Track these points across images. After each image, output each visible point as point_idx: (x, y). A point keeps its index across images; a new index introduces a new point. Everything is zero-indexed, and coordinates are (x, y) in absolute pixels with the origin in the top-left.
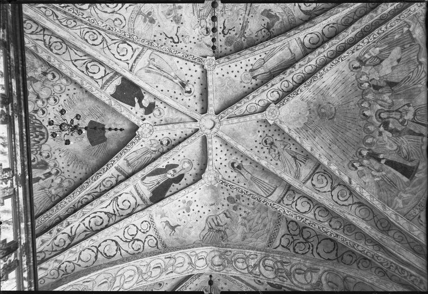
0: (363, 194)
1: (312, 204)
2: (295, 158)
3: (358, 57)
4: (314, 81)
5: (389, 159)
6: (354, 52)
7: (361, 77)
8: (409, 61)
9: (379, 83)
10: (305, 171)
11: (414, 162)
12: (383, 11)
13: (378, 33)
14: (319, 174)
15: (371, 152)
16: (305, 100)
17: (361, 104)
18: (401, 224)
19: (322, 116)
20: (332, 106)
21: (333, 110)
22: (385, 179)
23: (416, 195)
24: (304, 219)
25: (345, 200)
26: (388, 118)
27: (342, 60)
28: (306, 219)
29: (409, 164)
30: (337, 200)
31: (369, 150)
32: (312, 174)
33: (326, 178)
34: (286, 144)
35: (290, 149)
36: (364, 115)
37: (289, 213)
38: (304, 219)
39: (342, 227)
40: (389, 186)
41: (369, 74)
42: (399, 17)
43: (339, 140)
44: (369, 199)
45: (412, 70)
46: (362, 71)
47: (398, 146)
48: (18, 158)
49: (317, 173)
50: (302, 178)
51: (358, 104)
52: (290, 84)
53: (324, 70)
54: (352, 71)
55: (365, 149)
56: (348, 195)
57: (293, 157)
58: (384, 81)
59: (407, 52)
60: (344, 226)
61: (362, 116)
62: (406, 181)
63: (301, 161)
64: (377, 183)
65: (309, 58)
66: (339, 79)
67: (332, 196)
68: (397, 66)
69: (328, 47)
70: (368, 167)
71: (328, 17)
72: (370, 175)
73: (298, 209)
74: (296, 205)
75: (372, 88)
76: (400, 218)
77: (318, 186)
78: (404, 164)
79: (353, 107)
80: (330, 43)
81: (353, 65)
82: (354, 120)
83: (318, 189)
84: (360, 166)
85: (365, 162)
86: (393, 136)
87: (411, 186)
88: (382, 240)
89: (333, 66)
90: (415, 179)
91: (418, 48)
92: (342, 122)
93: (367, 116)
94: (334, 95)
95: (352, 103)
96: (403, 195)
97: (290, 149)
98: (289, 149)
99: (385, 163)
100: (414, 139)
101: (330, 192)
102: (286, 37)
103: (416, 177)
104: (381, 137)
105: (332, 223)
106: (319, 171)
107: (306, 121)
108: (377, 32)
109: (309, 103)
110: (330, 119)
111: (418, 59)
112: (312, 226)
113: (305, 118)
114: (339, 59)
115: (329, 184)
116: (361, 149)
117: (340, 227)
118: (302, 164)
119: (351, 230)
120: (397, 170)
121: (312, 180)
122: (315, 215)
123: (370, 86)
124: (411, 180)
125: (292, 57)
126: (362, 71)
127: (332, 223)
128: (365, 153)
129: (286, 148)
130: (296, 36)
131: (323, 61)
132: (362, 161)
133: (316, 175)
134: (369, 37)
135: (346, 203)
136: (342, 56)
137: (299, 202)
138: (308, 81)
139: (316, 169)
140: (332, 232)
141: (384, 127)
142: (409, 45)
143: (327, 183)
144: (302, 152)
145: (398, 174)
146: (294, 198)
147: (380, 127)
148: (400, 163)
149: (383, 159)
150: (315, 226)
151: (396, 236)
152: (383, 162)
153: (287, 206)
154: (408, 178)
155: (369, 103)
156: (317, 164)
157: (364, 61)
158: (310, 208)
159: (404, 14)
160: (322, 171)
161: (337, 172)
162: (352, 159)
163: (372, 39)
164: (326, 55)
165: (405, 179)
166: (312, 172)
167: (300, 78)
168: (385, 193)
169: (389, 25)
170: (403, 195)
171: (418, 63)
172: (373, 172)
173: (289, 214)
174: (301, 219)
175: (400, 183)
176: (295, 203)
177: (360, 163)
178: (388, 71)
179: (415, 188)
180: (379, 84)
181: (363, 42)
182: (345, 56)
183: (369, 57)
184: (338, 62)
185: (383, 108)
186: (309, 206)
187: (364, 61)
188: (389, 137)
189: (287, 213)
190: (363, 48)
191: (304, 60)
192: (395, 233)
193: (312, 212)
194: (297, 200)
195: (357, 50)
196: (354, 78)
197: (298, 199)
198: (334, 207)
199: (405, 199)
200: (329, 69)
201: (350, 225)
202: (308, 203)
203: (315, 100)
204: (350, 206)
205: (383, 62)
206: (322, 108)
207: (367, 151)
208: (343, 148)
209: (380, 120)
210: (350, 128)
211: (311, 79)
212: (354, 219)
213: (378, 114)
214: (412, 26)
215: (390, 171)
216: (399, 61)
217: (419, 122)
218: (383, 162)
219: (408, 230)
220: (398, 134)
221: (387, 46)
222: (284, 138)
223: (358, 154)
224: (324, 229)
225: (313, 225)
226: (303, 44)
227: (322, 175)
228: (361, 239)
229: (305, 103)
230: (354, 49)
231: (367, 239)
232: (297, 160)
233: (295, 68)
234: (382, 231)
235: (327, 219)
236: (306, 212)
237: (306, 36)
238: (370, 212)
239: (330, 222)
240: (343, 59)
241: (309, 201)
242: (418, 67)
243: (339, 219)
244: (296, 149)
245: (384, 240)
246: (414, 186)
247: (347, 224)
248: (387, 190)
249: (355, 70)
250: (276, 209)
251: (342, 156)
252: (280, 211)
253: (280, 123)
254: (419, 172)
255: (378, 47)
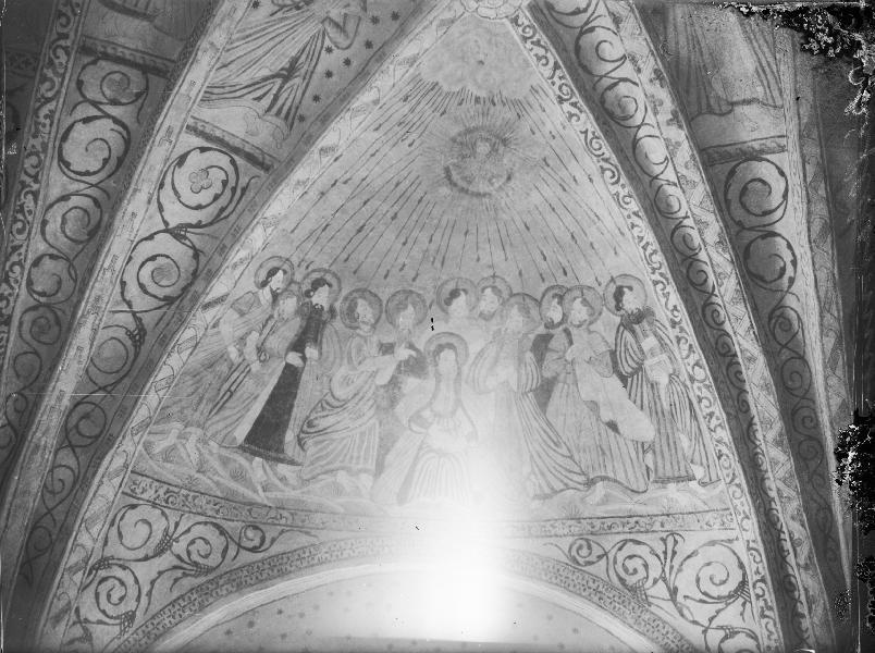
0: (175, 355)
1: (102, 175)
2: (288, 73)
3: (653, 314)
4: (603, 170)
5: (305, 377)
6: (673, 327)
7: (585, 302)
8: (604, 453)
9: (555, 356)
10: (238, 120)
11: (298, 447)
12: (774, 462)
13: (711, 415)
14: (230, 169)
15: (325, 316)
16: (531, 99)
17: (494, 288)
18: (99, 492)
19: (464, 144)
20: (497, 185)
21: (483, 187)
22: (236, 375)
23: (197, 475)
24: (35, 187)
25: (142, 286)
26: (438, 376)
27: (656, 283)
28: (35, 195)
29: (290, 436)
30: (139, 258)
31: (332, 311)
32: (227, 145)
33: (216, 197)
34: (350, 27)
35: (329, 50)
36: (454, 294)
37: (48, 122)
38: (35, 187)
39: (43, 300)
40: (216, 391)
41: (590, 332)
42: (739, 486)
43: (367, 206)
44: (160, 376)
45: (576, 458)
46: (605, 312)
47: (346, 401)
48: (48, 605)
49: (233, 162)
50: (206, 113)
51: (494, 276)
52: (610, 66)
53: (636, 214)
54: (612, 280)
55: (336, 300)
56: (161, 293)
57: (294, 61)
58: (558, 375)
59: (633, 455)
60: (47, 306)
61: (451, 286)
62: (236, 434)
63: (276, 98)
64: (223, 356)
65: (694, 185)
66: (594, 228)
67: (151, 237)
68: (598, 418)
69: (717, 258)
70: (271, 317)
71: (822, 294)
72: (244, 331)
73: (73, 134)
74: (87, 120)
75: (541, 330)
76: (116, 481)
77: (182, 179)
78: (288, 420)
79: (485, 260)
80: (729, 268)
81: (631, 288)
82: (439, 258)
83: (168, 180)
84: (272, 291)
85: (289, 305)
86: (377, 388)
87: (224, 452)
88: (35, 452)
89: (644, 248)
90: (246, 458)
91: (635, 488)
92: (435, 212)
93: (448, 302)
94: (535, 198)
95: (498, 256)
96: (193, 439)
97: (329, 50)
98: (327, 43)
99: (288, 366)
100: (368, 448)
101: (163, 227)
102: (805, 120)
103: (251, 461)
104: (374, 350)
105: (48, 264)
106: (241, 170)
107: (446, 88)
108: (717, 413)
109: (520, 107)
110: (447, 170)
111: (603, 478)
112: (15, 220)
113: (460, 80)
114: (661, 275)
115: (194, 217)
116: (335, 287)
117: (43, 294)
118: (266, 102)
119: (42, 331)
120: (269, 402)
121: (203, 150)
122: (64, 198)
123: (550, 325)
124: (241, 447)
125: (718, 98)
126: (605, 312)
127: (48, 264)
128: (321, 298)
129: (330, 30)
130: (792, 141)
131: (669, 205)
132: (292, 293)
133: (224, 161)
134: (708, 387)
135: (133, 291)
136: (669, 289)
137: (104, 128)
138: (604, 150)
139: (250, 158)
140: (12, 299)
141: (407, 362)
142: (651, 466)
143: (199, 207)
144: (316, 98)
145: (257, 409)
146: (114, 102)
147: (411, 346)
148: (292, 406)
149: (304, 359)
150: (20, 232)
151: (62, 473)
152: (294, 359)
153: (73, 85)
154: (248, 439)
155: (492, 315)
156: (268, 161)
157: (636, 327)
158: (87, 173)
159: (743, 499)
160: (243, 181)
161: (243, 254)
162: (296, 263)
163: (698, 393)
164: (686, 222)
165: (242, 431)
166: (236, 143)
167: (623, 109)
168: (190, 390)
169: (725, 450)
170: (193, 439)
171: (591, 477)
172: (255, 335)
173: (42, 120)
174: (32, 172)
175: (229, 421)
176: (93, 112)
177: (286, 290)
178: (586, 392)
179: (216, 464)
180: (550, 356)
181: (697, 364)
182: (667, 295)
183: (645, 349)
184: (654, 270)
185: (470, 361)
186: (95, 165)
187: (636, 327)
188: (374, 375)
189: (45, 111)
190: (678, 357)
191: (691, 164)
192: (72, 470)
193: (75, 187)
194: (108, 116)
195: (679, 340)
196: (589, 281)
197: (116, 121)
198: (108, 274)
199: (182, 450)
200: (636, 231)
201: (58, 322)
202: (106, 161)
203: (526, 131)
204: (126, 308)
205: (619, 382)
206: (494, 149)
207: (326, 308)
208: (335, 225)
209: (432, 348)
210: (410, 241)
211: (614, 160)
212: (80, 349)
213: (453, 340)
214: (701, 490)
215: (265, 385)
216: (613, 426)
217: (419, 467)
218: (294, 359)
219: (88, 514)
220: (385, 403)
221: (666, 407)
222: (375, 20)
223: (316, 276)
224: (17, 269)
225: (19, 225)
226: (756, 156)
227: (225, 183)
228: (18, 376)
229: (522, 93)
230: (682, 330)
231: (27, 392)
232: (279, 81)
233: (669, 123)
234: (65, 430)
235: (58, 244)
236: (68, 165)
237: (782, 173)
238: (117, 372)
239: (52, 257)
240: (660, 286)
241: (113, 162)
242: (583, 474)
243: (68, 285)
244: (329, 74)
245: (38, 457)
246: (225, 461)
247: (59, 313)
248: (200, 390)
249: (612, 289)
250: (51, 63)
251: (308, 226)
252: (44, 79)
253: (443, 23)
254: (267, 468)
255: (670, 382)
